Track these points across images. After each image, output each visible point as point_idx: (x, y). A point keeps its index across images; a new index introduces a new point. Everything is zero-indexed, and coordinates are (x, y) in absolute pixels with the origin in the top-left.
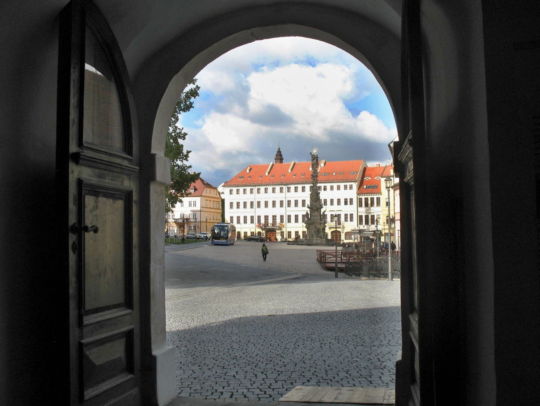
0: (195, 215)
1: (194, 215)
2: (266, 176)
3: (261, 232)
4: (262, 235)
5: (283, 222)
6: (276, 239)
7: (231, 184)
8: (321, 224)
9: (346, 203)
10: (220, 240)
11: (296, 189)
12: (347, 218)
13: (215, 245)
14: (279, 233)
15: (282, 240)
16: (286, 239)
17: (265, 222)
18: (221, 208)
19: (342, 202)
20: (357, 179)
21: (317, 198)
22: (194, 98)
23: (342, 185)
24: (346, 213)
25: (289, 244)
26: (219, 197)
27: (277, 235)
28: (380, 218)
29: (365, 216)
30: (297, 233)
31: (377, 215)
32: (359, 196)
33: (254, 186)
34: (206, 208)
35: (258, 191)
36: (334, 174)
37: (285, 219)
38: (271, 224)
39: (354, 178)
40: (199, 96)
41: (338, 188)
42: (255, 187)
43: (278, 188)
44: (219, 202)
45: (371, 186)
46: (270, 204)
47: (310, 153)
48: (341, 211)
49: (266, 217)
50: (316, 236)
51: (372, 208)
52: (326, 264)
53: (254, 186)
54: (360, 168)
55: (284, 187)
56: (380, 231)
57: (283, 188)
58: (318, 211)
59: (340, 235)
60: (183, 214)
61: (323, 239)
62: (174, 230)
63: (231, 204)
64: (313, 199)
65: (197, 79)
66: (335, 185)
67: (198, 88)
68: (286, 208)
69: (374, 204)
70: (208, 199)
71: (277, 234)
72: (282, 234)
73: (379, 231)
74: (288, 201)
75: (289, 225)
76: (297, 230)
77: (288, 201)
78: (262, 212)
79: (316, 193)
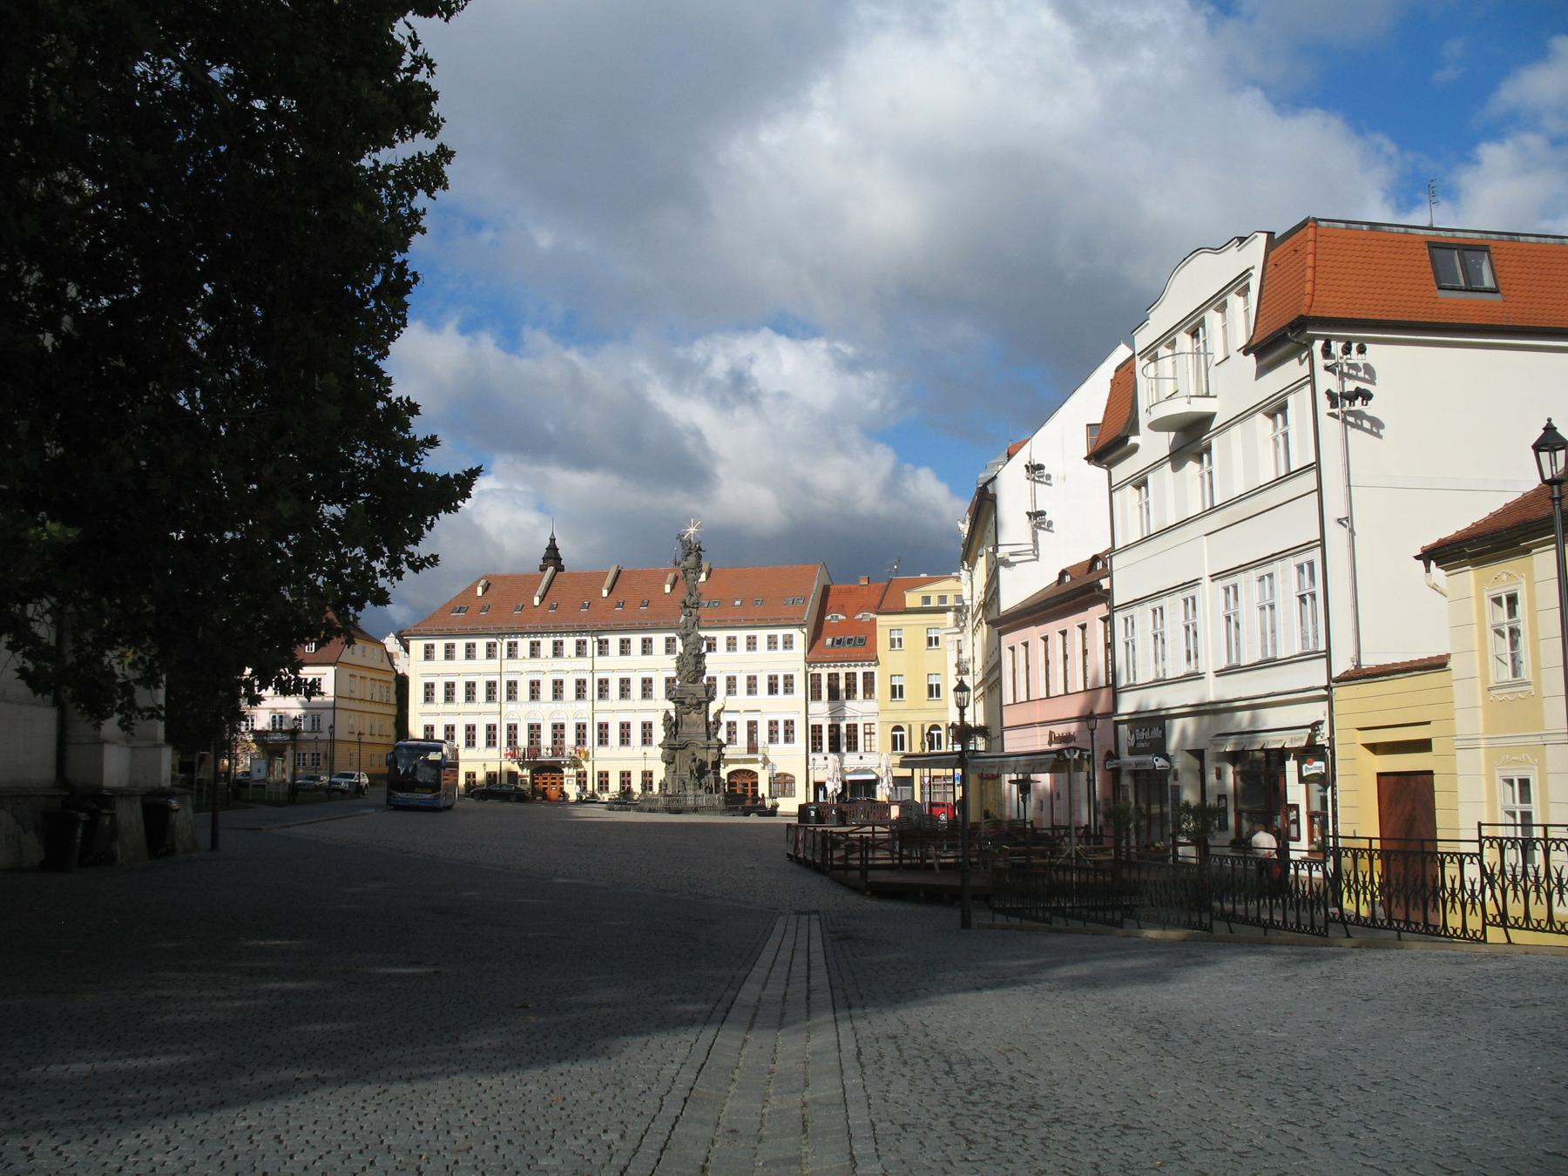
0: (319, 720)
1: (313, 720)
2: (535, 606)
3: (516, 773)
4: (521, 783)
5: (584, 743)
6: (564, 793)
7: (428, 628)
8: (708, 748)
9: (772, 689)
10: (413, 792)
11: (625, 647)
12: (777, 732)
13: (398, 808)
14: (573, 776)
15: (581, 797)
16: (593, 795)
17: (531, 743)
18: (393, 700)
19: (763, 685)
20: (805, 619)
21: (698, 671)
22: (429, 195)
23: (762, 635)
24: (773, 718)
25: (613, 810)
26: (390, 669)
27: (565, 783)
28: (874, 733)
29: (830, 726)
30: (625, 776)
31: (865, 724)
32: (810, 669)
33: (497, 635)
34: (350, 698)
35: (509, 650)
36: (738, 603)
37: (591, 735)
38: (547, 749)
39: (799, 616)
40: (446, 187)
41: (749, 644)
42: (500, 640)
43: (570, 643)
44: (390, 682)
45: (846, 640)
46: (546, 690)
47: (679, 535)
48: (759, 711)
49: (534, 729)
50: (695, 784)
51: (849, 704)
52: (871, 873)
53: (499, 634)
54: (815, 589)
55: (589, 639)
56: (1078, 752)
57: (585, 643)
58: (699, 709)
59: (755, 784)
60: (281, 717)
61: (716, 793)
62: (245, 761)
63: (429, 688)
64: (684, 673)
65: (443, 120)
66: (741, 636)
67: (445, 154)
68: (593, 700)
69: (855, 691)
70: (358, 673)
71: (565, 779)
72: (581, 779)
73: (1075, 753)
74: (600, 682)
75: (601, 752)
76: (625, 769)
77: (600, 682)
78: (521, 713)
79: (695, 655)
